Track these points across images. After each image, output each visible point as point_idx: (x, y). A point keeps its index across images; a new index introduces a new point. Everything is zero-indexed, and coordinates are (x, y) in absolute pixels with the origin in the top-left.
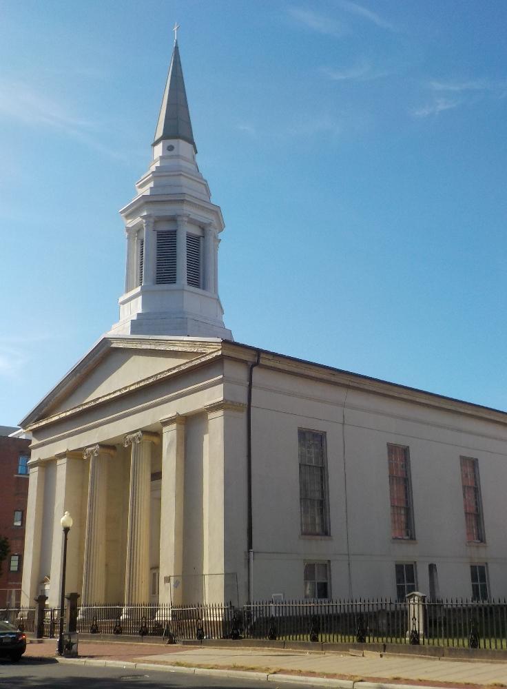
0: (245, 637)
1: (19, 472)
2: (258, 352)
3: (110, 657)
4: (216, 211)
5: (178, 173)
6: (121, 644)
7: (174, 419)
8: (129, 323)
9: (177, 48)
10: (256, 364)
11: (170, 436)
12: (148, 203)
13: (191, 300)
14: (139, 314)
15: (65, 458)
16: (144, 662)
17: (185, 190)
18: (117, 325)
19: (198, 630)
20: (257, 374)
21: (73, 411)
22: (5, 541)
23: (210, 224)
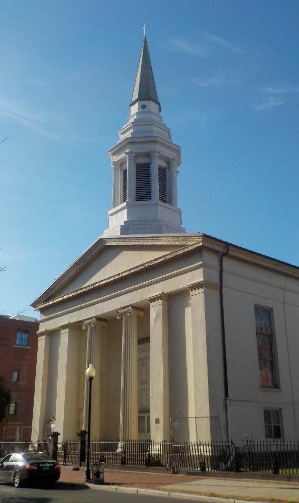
0: (247, 471)
1: (17, 344)
2: (228, 245)
3: (132, 484)
4: (177, 150)
5: (152, 123)
6: (127, 473)
7: (44, 333)
8: (119, 228)
9: (145, 40)
10: (226, 254)
11: (156, 310)
12: (130, 143)
13: (162, 212)
14: (125, 222)
15: (202, 287)
16: (176, 491)
17: (155, 135)
18: (107, 230)
19: (101, 456)
20: (224, 259)
21: (75, 293)
22: (8, 393)
23: (174, 159)
